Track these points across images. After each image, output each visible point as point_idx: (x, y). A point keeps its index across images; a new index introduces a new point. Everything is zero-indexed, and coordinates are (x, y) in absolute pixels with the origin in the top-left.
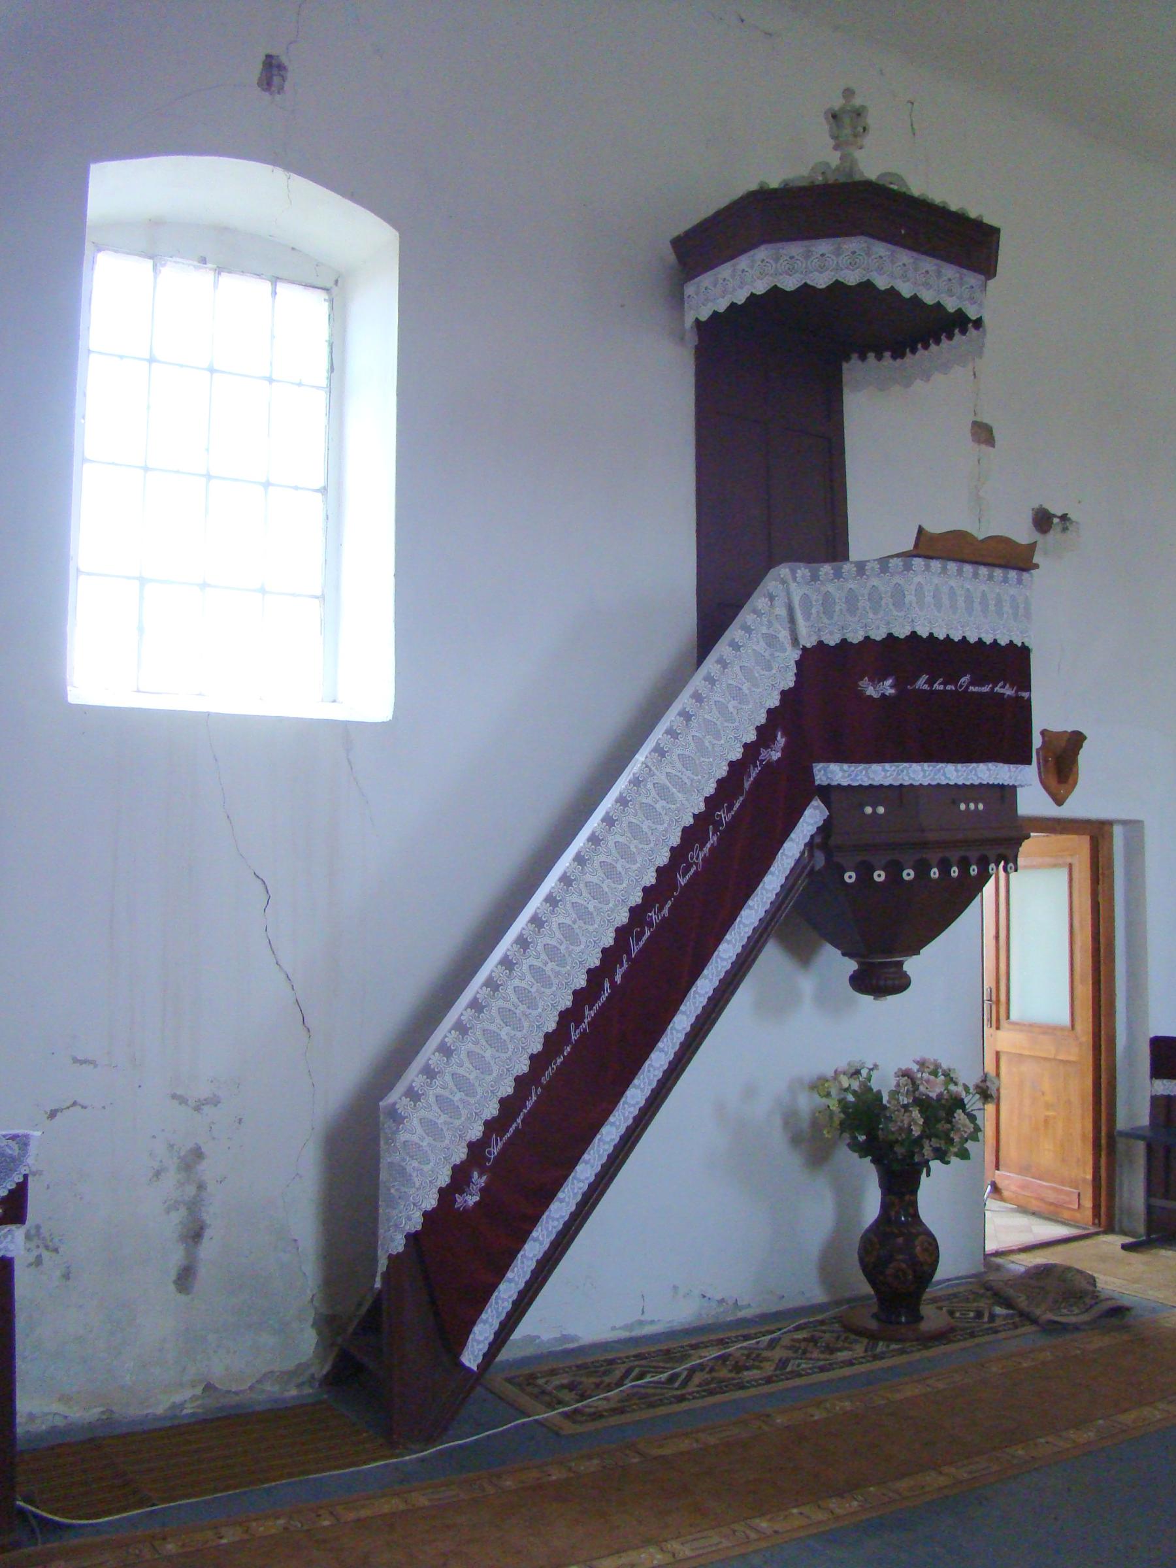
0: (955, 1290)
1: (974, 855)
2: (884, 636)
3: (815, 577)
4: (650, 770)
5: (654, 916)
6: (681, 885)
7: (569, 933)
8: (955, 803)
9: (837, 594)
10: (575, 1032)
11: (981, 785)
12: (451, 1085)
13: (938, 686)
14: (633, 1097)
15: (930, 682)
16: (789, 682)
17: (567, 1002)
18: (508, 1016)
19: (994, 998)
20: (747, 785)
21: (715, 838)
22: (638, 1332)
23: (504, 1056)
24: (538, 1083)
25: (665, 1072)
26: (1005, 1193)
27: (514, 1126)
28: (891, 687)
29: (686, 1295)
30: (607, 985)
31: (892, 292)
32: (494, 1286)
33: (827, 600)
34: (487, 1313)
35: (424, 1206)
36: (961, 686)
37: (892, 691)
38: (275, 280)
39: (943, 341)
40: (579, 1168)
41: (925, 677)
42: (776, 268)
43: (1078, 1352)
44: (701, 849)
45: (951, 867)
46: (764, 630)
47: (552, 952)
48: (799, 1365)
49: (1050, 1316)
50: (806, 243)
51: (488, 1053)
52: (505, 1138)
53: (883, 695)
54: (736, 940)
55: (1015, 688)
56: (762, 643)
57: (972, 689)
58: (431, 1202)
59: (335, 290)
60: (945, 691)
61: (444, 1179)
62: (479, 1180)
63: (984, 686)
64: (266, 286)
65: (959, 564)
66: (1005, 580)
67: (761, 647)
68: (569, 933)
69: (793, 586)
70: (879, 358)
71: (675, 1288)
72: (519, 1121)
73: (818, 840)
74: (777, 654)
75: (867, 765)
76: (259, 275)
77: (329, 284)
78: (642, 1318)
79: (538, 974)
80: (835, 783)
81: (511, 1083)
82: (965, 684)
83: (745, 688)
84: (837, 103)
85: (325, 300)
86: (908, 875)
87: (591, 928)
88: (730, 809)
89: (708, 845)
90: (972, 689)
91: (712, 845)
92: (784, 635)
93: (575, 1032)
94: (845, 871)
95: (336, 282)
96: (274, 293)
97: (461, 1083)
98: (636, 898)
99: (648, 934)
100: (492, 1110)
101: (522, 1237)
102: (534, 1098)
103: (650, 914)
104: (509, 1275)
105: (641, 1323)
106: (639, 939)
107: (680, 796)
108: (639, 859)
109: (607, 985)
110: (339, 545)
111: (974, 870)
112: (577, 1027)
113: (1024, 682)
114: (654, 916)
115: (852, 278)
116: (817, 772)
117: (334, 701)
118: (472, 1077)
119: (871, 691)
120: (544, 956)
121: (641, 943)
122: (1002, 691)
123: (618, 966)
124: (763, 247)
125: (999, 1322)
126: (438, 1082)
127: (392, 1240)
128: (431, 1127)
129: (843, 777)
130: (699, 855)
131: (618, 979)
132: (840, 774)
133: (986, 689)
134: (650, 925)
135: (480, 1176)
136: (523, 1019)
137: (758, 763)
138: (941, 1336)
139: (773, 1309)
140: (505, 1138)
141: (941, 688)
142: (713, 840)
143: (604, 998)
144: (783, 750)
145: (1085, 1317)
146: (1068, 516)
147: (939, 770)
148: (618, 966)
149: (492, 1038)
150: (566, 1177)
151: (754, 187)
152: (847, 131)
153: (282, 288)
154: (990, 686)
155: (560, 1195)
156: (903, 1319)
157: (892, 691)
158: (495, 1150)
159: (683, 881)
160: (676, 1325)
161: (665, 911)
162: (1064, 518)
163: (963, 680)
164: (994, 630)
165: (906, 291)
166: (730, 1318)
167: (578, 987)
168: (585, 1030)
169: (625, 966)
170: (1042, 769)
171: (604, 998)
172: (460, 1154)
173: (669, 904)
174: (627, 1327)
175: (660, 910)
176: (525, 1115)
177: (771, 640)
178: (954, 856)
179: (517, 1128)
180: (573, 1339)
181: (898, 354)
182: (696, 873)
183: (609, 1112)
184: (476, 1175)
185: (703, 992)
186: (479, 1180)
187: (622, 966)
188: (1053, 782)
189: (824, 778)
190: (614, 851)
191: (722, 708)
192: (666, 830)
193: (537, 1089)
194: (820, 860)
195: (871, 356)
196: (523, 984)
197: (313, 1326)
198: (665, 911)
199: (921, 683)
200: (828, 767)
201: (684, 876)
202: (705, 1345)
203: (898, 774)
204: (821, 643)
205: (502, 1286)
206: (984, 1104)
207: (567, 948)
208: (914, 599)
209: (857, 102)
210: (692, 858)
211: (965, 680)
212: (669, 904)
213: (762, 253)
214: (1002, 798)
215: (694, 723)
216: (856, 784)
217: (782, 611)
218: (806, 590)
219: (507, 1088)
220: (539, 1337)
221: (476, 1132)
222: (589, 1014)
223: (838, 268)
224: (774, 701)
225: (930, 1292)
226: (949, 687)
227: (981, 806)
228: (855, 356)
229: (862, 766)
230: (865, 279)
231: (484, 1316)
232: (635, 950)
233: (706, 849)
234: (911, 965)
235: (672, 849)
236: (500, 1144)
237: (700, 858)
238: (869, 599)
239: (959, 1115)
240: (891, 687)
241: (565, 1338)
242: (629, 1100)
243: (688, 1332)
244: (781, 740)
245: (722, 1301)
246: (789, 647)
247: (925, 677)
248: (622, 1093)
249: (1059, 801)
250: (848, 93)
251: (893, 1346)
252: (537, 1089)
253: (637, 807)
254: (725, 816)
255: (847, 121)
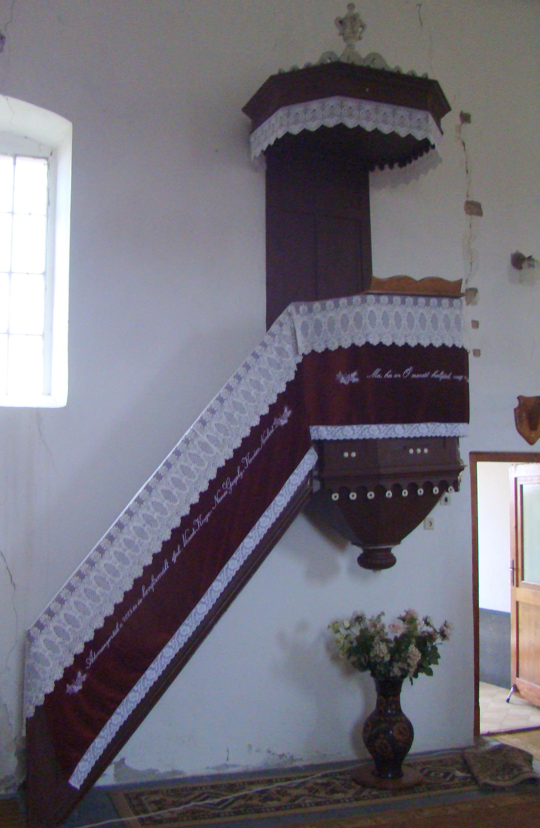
0: (442, 758)
1: (421, 482)
2: (350, 345)
3: (310, 310)
4: (196, 433)
5: (198, 522)
6: (217, 503)
7: (141, 532)
8: (406, 449)
9: (324, 321)
10: (145, 590)
11: (421, 438)
12: (64, 621)
13: (388, 375)
14: (184, 631)
15: (383, 373)
16: (292, 377)
17: (139, 573)
18: (101, 581)
19: (515, 567)
20: (263, 441)
21: (241, 474)
22: (222, 771)
23: (98, 605)
24: (120, 621)
25: (189, 639)
26: (522, 693)
27: (105, 645)
28: (356, 377)
29: (258, 751)
30: (166, 563)
31: (359, 129)
32: (92, 740)
33: (318, 325)
34: (87, 755)
35: (45, 690)
36: (405, 375)
37: (357, 380)
38: (15, 156)
39: (424, 154)
40: (148, 672)
41: (378, 370)
42: (359, 113)
43: (492, 807)
44: (232, 480)
45: (433, 487)
46: (276, 345)
47: (129, 543)
48: (305, 800)
49: (488, 781)
50: (304, 104)
51: (88, 603)
52: (99, 653)
53: (351, 383)
54: (256, 536)
55: (450, 374)
56: (275, 353)
57: (414, 376)
58: (50, 689)
59: (51, 158)
60: (393, 379)
61: (59, 675)
62: (81, 677)
63: (424, 373)
64: (10, 160)
65: (402, 297)
66: (440, 305)
67: (274, 356)
68: (141, 532)
69: (295, 316)
70: (391, 167)
71: (250, 746)
72: (108, 643)
73: (315, 473)
74: (284, 359)
75: (342, 427)
76: (6, 154)
77: (48, 155)
78: (228, 763)
79: (121, 557)
80: (322, 438)
81: (102, 621)
82: (409, 373)
83: (262, 381)
84: (343, 13)
85: (44, 165)
86: (371, 495)
87: (155, 529)
88: (251, 456)
89: (237, 478)
90: (414, 376)
91: (240, 478)
92: (288, 347)
93: (145, 590)
94: (332, 493)
95: (51, 154)
96: (15, 163)
97: (70, 620)
98: (186, 511)
99: (194, 533)
100: (89, 636)
101: (110, 712)
102: (118, 630)
103: (196, 521)
104: (102, 734)
105: (227, 766)
106: (188, 535)
107: (215, 449)
108: (188, 488)
109: (166, 563)
110: (52, 305)
111: (436, 490)
112: (146, 589)
113: (464, 370)
114: (198, 522)
115: (331, 123)
116: (313, 432)
117: (49, 394)
118: (77, 617)
119: (343, 380)
120: (124, 545)
121: (190, 538)
122: (437, 376)
123: (174, 551)
124: (281, 109)
125: (456, 781)
126: (56, 618)
127: (28, 709)
128: (50, 644)
129: (328, 434)
130: (230, 484)
131: (174, 559)
132: (326, 433)
133: (425, 375)
134: (196, 527)
135: (82, 675)
136: (110, 583)
137: (272, 427)
138: (411, 788)
139: (316, 762)
140: (99, 653)
141: (391, 376)
142: (240, 475)
143: (164, 571)
144: (289, 419)
145: (509, 783)
146: (533, 257)
147: (391, 429)
148: (174, 551)
149: (90, 593)
150: (138, 678)
151: (275, 72)
152: (348, 30)
153: (19, 160)
154: (429, 373)
155: (135, 688)
156: (390, 775)
157: (357, 380)
158: (92, 659)
159: (218, 500)
160: (250, 769)
161: (207, 519)
162: (530, 258)
163: (406, 371)
164: (430, 337)
165: (369, 127)
166: (288, 766)
167: (147, 564)
168: (151, 590)
169: (179, 552)
170: (518, 421)
171: (164, 571)
172: (70, 661)
173: (208, 515)
174: (217, 768)
175: (203, 518)
176: (112, 640)
177: (281, 351)
178: (404, 482)
179: (106, 647)
180: (180, 773)
181: (402, 164)
182: (227, 495)
183: (167, 640)
184: (79, 674)
185: (248, 546)
186: (81, 677)
187: (177, 551)
188: (526, 428)
189: (317, 435)
190: (171, 483)
191: (246, 395)
192: (206, 470)
193: (119, 624)
194: (317, 486)
195: (386, 166)
196: (110, 562)
197: (15, 754)
198: (207, 519)
199: (376, 374)
200: (319, 428)
201: (219, 497)
202: (258, 783)
203: (388, 431)
204: (313, 351)
205: (97, 740)
206: (442, 640)
207: (139, 541)
208: (368, 321)
209: (356, 11)
210: (225, 486)
211: (408, 371)
212: (208, 515)
213: (281, 113)
214: (444, 446)
215: (226, 404)
216: (335, 439)
217: (287, 332)
218: (305, 318)
219: (100, 623)
220: (157, 770)
221: (79, 648)
222: (154, 581)
223: (340, 116)
224: (282, 388)
225: (407, 759)
226: (396, 376)
227: (426, 451)
228: (377, 168)
229: (339, 428)
230: (339, 122)
231: (85, 757)
232: (186, 542)
233: (235, 481)
234: (396, 551)
235: (210, 482)
236: (96, 656)
237: (231, 486)
238: (383, 319)
239: (412, 648)
240: (356, 377)
241: (174, 772)
242: (245, 545)
243: (254, 773)
244: (287, 413)
245: (282, 756)
246: (291, 355)
247: (378, 370)
248: (177, 628)
249: (531, 442)
250: (351, 6)
251: (374, 792)
252: (119, 624)
253: (187, 455)
254: (248, 461)
255: (348, 23)
